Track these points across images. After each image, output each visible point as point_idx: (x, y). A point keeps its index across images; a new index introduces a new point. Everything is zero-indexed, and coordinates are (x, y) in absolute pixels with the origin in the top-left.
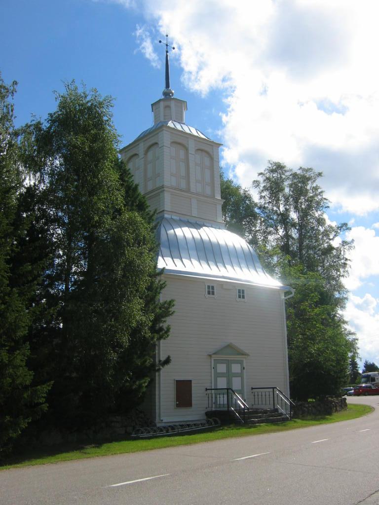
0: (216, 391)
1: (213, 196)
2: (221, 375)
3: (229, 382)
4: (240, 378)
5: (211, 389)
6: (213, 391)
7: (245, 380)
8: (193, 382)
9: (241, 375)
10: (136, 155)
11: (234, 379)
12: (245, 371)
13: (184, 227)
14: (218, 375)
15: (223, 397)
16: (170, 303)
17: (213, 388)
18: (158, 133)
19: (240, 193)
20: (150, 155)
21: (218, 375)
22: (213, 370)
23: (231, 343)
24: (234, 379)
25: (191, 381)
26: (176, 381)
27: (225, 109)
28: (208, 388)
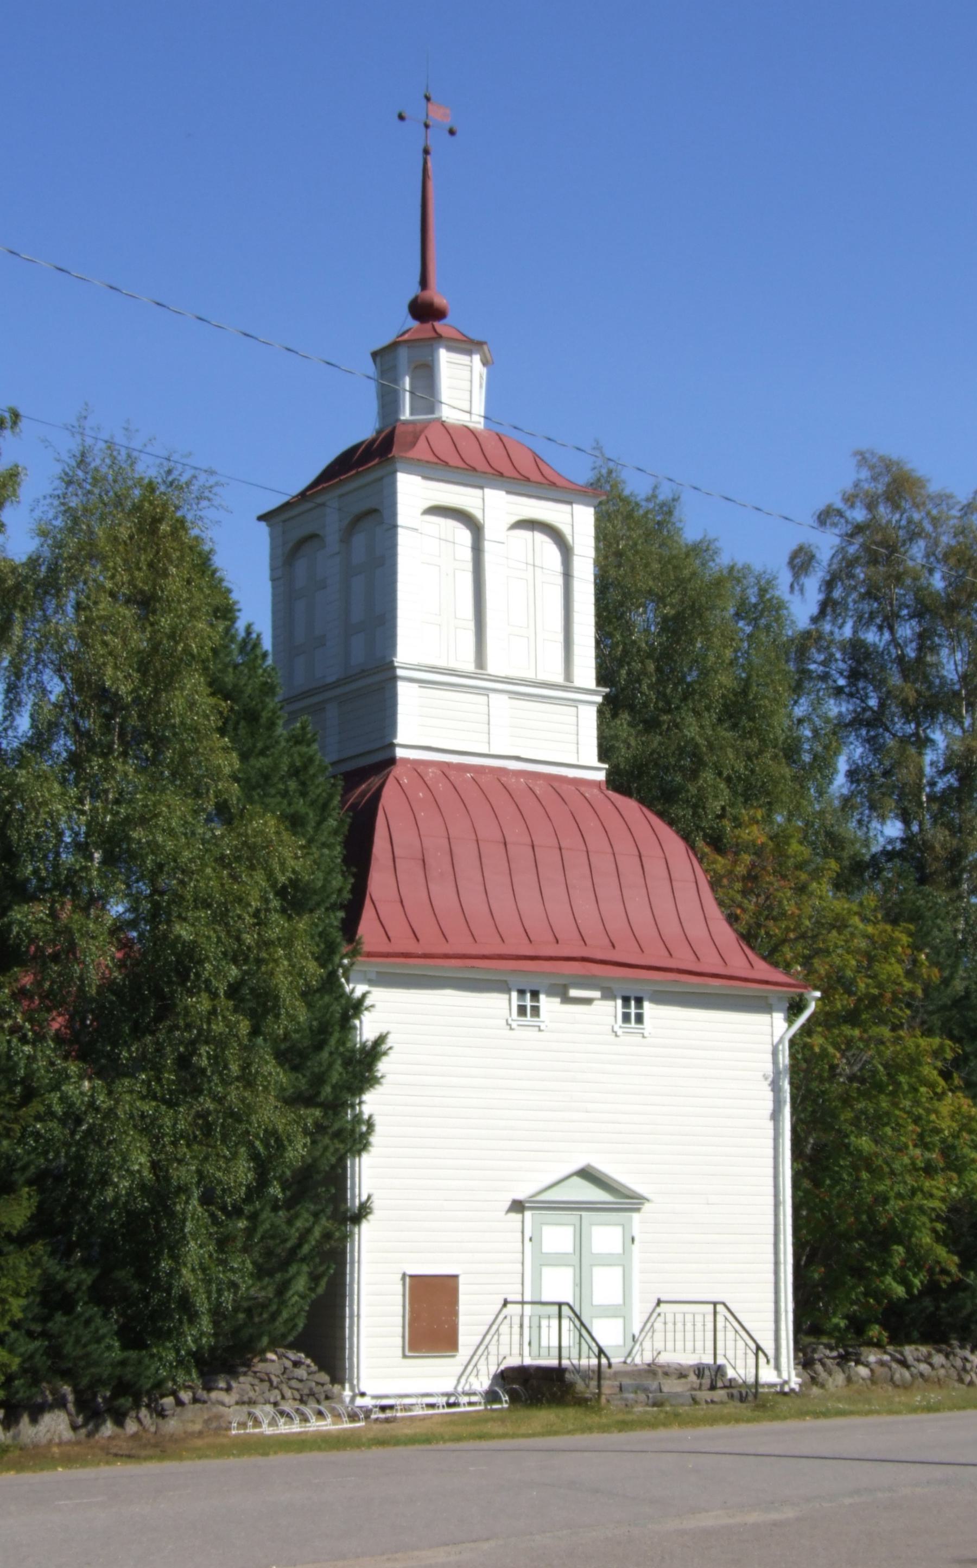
0: (539, 1308)
1: (568, 683)
2: (557, 1260)
3: (580, 1283)
4: (619, 1270)
5: (523, 1303)
6: (528, 1308)
7: (636, 1277)
8: (461, 1280)
9: (623, 1261)
10: (313, 537)
11: (597, 1271)
12: (636, 1248)
13: (578, 503)
14: (545, 1260)
15: (560, 1358)
16: (370, 1117)
17: (528, 1298)
18: (381, 479)
19: (899, 1299)
20: (359, 540)
21: (545, 1260)
22: (528, 1244)
23: (589, 1166)
24: (597, 1271)
25: (455, 1277)
26: (411, 1276)
27: (372, 1086)
28: (510, 1298)
